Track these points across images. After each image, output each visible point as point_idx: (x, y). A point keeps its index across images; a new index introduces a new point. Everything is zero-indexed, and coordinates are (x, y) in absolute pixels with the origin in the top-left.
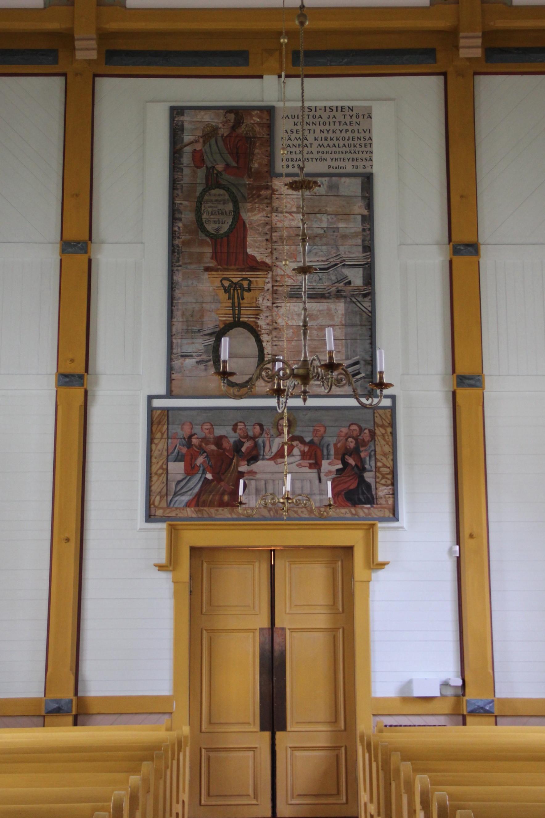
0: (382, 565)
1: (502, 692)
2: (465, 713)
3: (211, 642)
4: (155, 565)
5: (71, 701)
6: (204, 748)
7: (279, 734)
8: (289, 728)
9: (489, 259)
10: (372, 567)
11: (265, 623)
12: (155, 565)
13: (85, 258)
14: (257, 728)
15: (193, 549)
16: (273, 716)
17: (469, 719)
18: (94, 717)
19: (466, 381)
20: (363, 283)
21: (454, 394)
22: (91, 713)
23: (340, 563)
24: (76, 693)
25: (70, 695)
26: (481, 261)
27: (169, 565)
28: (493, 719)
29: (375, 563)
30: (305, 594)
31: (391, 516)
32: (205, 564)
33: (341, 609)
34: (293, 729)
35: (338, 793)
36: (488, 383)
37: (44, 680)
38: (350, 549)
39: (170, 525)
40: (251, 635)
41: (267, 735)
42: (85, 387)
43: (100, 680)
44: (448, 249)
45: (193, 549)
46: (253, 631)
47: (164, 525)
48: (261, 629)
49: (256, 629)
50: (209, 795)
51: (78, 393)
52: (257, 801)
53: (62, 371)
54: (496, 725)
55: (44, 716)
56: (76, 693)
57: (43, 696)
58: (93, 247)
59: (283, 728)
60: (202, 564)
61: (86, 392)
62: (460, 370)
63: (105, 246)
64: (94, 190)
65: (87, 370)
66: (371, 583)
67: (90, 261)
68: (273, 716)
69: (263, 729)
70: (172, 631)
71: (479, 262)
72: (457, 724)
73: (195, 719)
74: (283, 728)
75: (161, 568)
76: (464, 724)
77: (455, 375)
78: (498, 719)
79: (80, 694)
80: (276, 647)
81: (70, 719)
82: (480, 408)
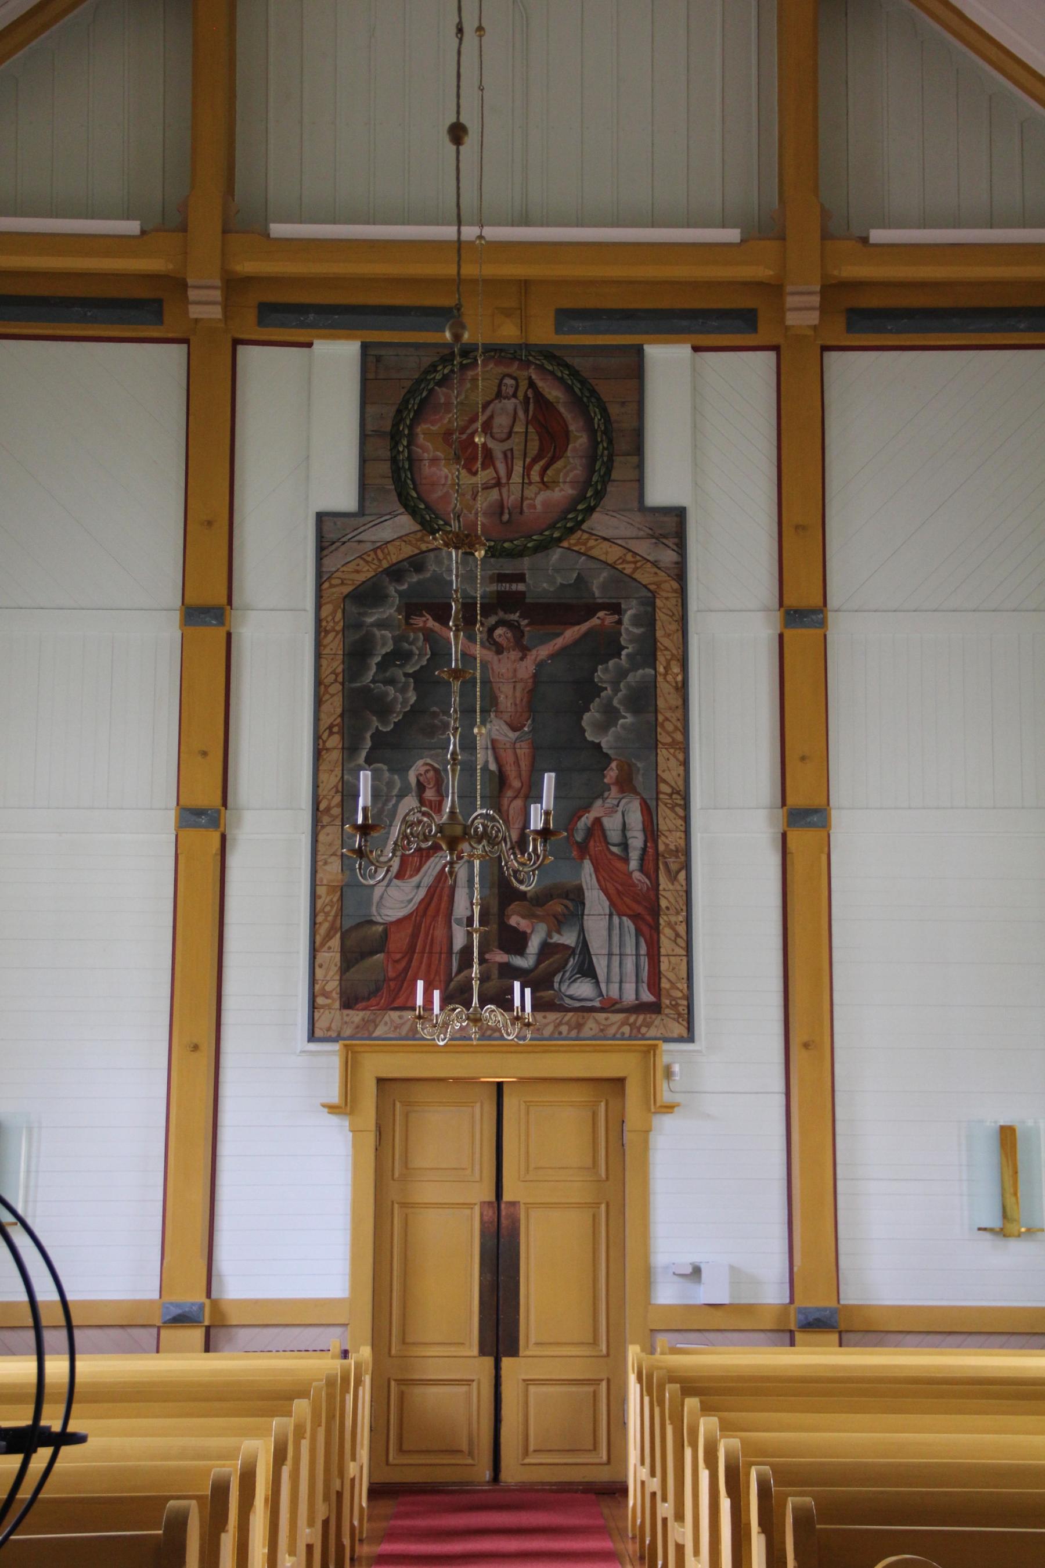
0: (669, 1108)
1: (851, 1296)
2: (793, 1328)
3: (407, 1131)
4: (324, 1106)
5: (202, 1306)
6: (395, 1380)
7: (506, 1362)
8: (521, 1353)
9: (842, 630)
10: (653, 1110)
11: (490, 1196)
12: (324, 1106)
13: (222, 633)
14: (475, 1351)
15: (380, 1081)
16: (500, 1334)
17: (798, 1336)
18: (234, 1330)
19: (803, 816)
20: (643, 350)
21: (784, 836)
22: (229, 1323)
23: (603, 1104)
24: (209, 1295)
25: (200, 1298)
26: (831, 832)
27: (345, 1106)
28: (835, 1337)
29: (658, 1104)
30: (550, 1143)
31: (685, 1034)
32: (398, 1105)
33: (603, 1175)
34: (528, 1353)
35: (595, 1447)
36: (837, 817)
37: (172, 896)
38: (618, 1083)
39: (346, 1046)
40: (468, 1212)
41: (489, 1361)
42: (222, 829)
43: (241, 1280)
44: (777, 616)
45: (380, 1081)
46: (470, 1206)
47: (336, 1047)
48: (483, 1203)
49: (473, 1381)
50: (401, 1450)
51: (216, 634)
52: (473, 1459)
53: (193, 600)
54: (841, 1345)
55: (159, 1328)
56: (209, 1295)
57: (158, 1297)
58: (235, 615)
59: (514, 1352)
60: (394, 1104)
61: (223, 838)
62: (790, 601)
63: (252, 615)
64: (235, 525)
65: (225, 804)
66: (651, 1133)
67: (229, 635)
68: (500, 1334)
69: (483, 1352)
70: (350, 1188)
71: (825, 636)
72: (783, 1345)
73: (379, 1340)
74: (514, 1352)
75: (332, 1109)
76: (792, 1344)
77: (785, 808)
78: (845, 1336)
79: (214, 1295)
80: (504, 1222)
81: (197, 1335)
82: (824, 857)
